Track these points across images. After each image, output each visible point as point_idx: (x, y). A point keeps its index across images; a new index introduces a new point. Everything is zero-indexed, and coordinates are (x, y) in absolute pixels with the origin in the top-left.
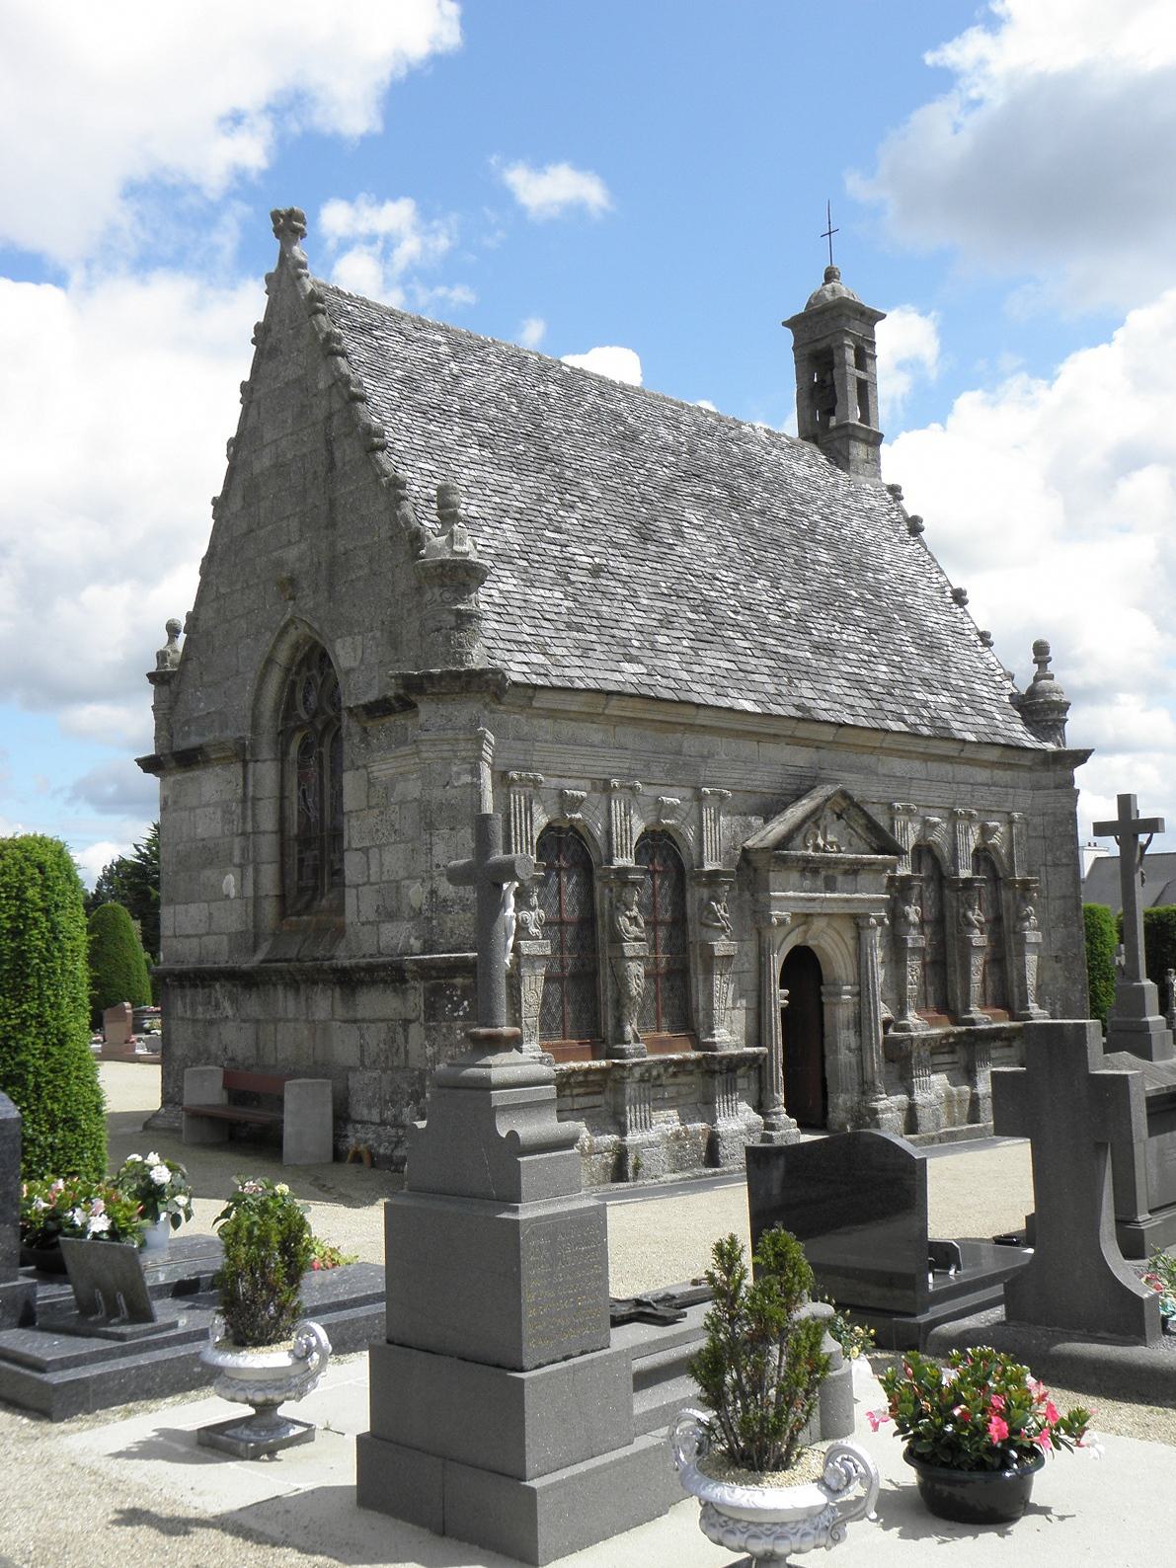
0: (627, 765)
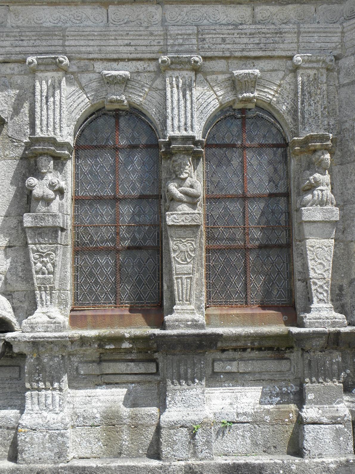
0: (97, 43)
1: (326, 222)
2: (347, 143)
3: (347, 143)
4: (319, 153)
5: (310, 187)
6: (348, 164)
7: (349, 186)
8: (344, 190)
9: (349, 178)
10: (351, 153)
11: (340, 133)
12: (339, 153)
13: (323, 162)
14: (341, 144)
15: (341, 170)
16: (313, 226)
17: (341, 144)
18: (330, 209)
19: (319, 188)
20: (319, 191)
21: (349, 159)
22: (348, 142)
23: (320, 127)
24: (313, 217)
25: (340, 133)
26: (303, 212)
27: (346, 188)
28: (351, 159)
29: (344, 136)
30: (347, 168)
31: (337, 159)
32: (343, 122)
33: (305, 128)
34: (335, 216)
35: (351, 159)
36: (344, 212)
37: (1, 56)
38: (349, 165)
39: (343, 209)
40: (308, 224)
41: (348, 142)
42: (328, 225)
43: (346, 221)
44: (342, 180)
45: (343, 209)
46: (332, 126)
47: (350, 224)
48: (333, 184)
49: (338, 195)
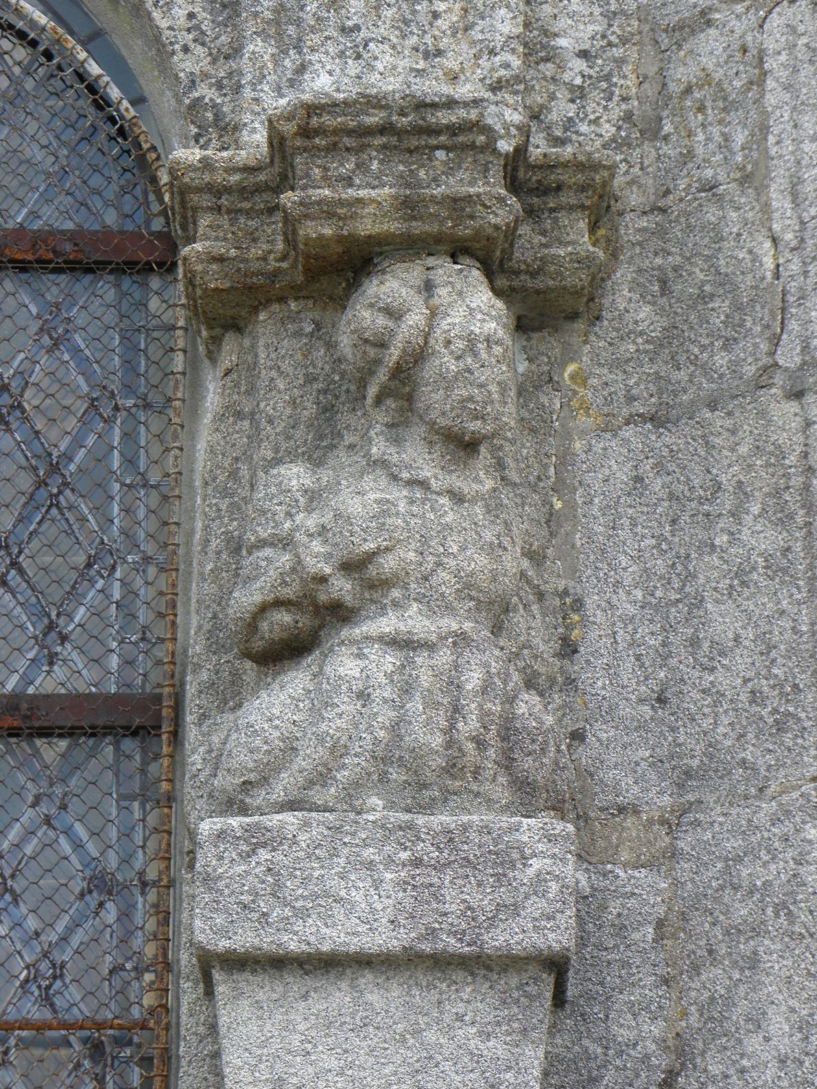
1: (441, 963)
2: (711, 214)
3: (711, 214)
4: (393, 285)
5: (305, 622)
6: (713, 406)
7: (723, 620)
8: (682, 659)
9: (722, 540)
10: (738, 308)
11: (652, 132)
12: (645, 312)
13: (428, 371)
14: (661, 232)
15: (659, 468)
16: (317, 1004)
17: (661, 232)
18: (485, 829)
19: (387, 624)
20: (372, 652)
21: (721, 360)
22: (720, 199)
23: (451, 62)
24: (303, 914)
25: (652, 132)
26: (206, 858)
27: (694, 642)
28: (735, 366)
29: (690, 154)
30: (709, 446)
31: (617, 364)
32: (680, 27)
33: (302, 69)
34: (535, 906)
35: (735, 366)
36: (677, 884)
37: (18, 301)
38: (718, 420)
39: (673, 854)
40: (263, 989)
41: (720, 199)
42: (471, 1002)
43: (696, 969)
44: (660, 565)
45: (673, 854)
46: (579, 65)
47: (729, 1002)
48: (578, 605)
49: (625, 710)
